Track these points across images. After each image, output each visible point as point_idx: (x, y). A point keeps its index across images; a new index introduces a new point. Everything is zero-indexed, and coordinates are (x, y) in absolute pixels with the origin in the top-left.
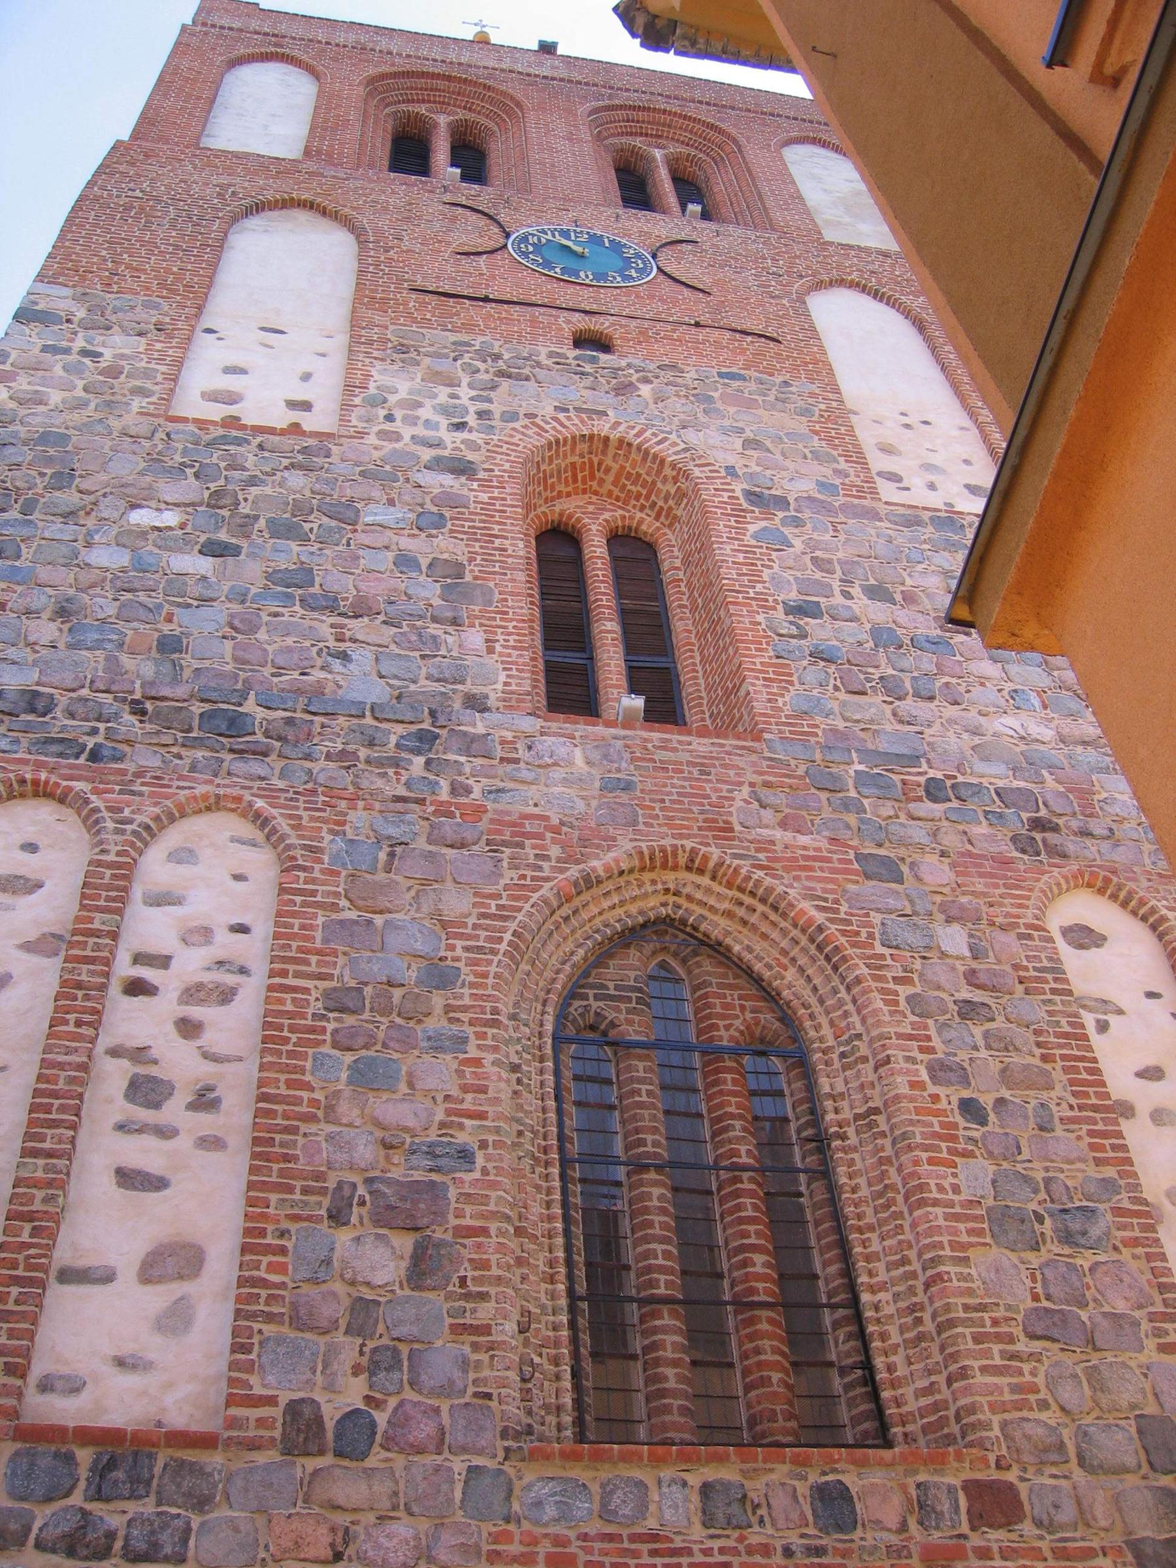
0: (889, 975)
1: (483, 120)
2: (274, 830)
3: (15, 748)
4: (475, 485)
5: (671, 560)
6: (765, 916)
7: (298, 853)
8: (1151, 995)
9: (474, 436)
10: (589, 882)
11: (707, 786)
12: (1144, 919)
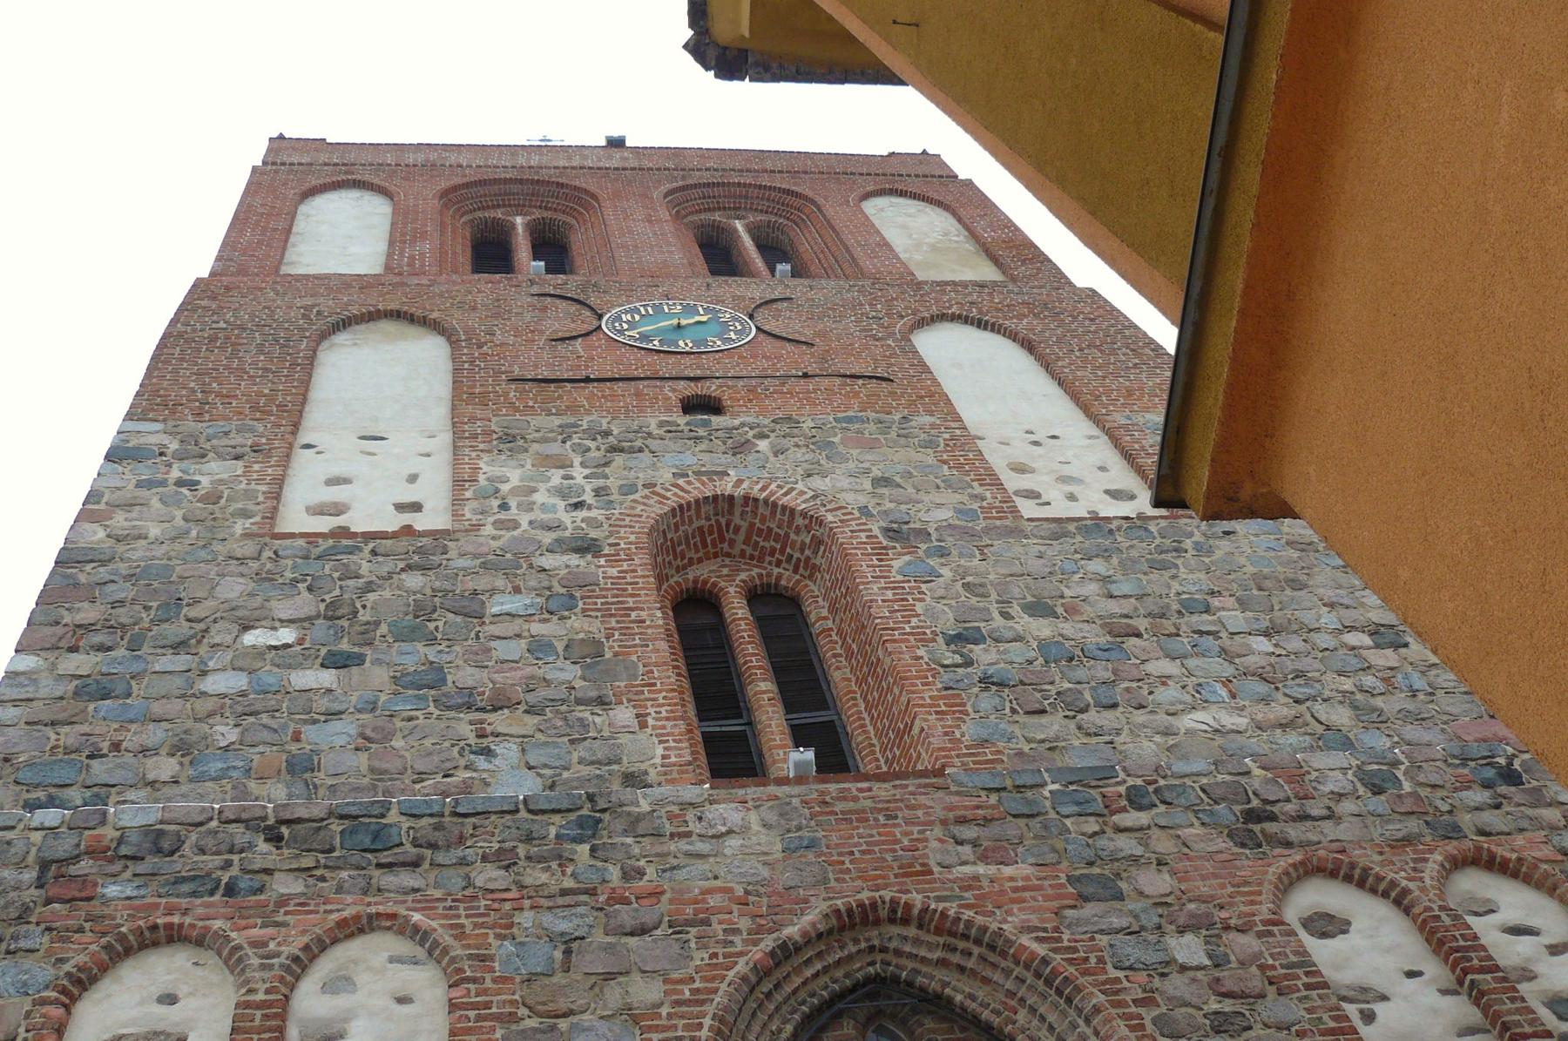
0: (1128, 999)
1: (561, 217)
2: (436, 944)
3: (142, 892)
4: (602, 561)
5: (817, 611)
6: (982, 958)
7: (466, 965)
8: (1411, 974)
9: (594, 513)
10: (785, 952)
11: (897, 831)
12: (1385, 895)
